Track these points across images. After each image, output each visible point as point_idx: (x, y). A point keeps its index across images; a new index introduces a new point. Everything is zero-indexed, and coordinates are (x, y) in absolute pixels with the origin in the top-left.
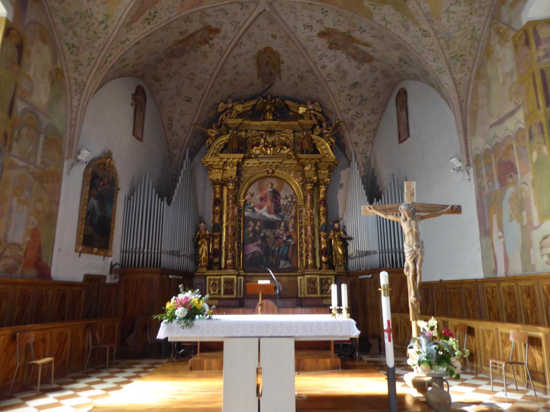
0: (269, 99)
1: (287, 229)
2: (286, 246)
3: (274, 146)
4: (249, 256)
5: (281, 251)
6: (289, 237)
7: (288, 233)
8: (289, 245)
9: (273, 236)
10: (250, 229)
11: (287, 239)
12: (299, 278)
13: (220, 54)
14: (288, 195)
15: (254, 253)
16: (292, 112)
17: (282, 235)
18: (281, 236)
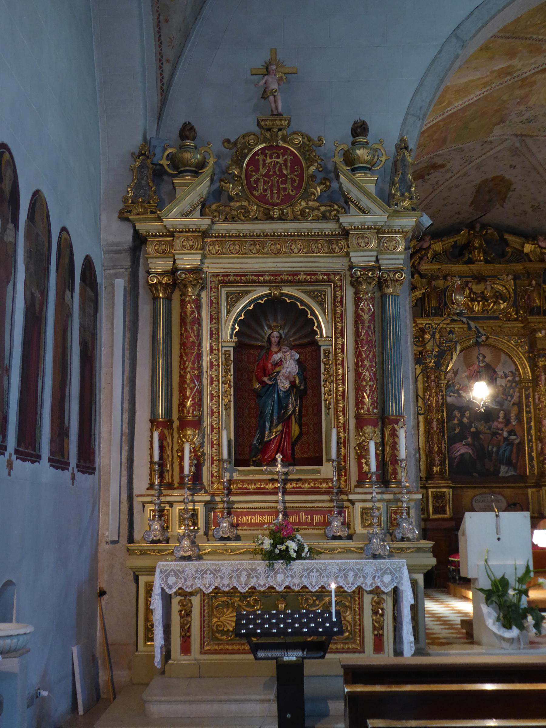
0: (478, 229)
1: (508, 422)
2: (507, 445)
3: (485, 299)
4: (456, 460)
5: (500, 452)
6: (512, 432)
7: (510, 427)
8: (511, 444)
9: (488, 431)
10: (456, 421)
11: (508, 436)
12: (530, 491)
13: (433, 188)
14: (507, 372)
15: (462, 455)
16: (511, 247)
17: (502, 430)
18: (500, 432)
